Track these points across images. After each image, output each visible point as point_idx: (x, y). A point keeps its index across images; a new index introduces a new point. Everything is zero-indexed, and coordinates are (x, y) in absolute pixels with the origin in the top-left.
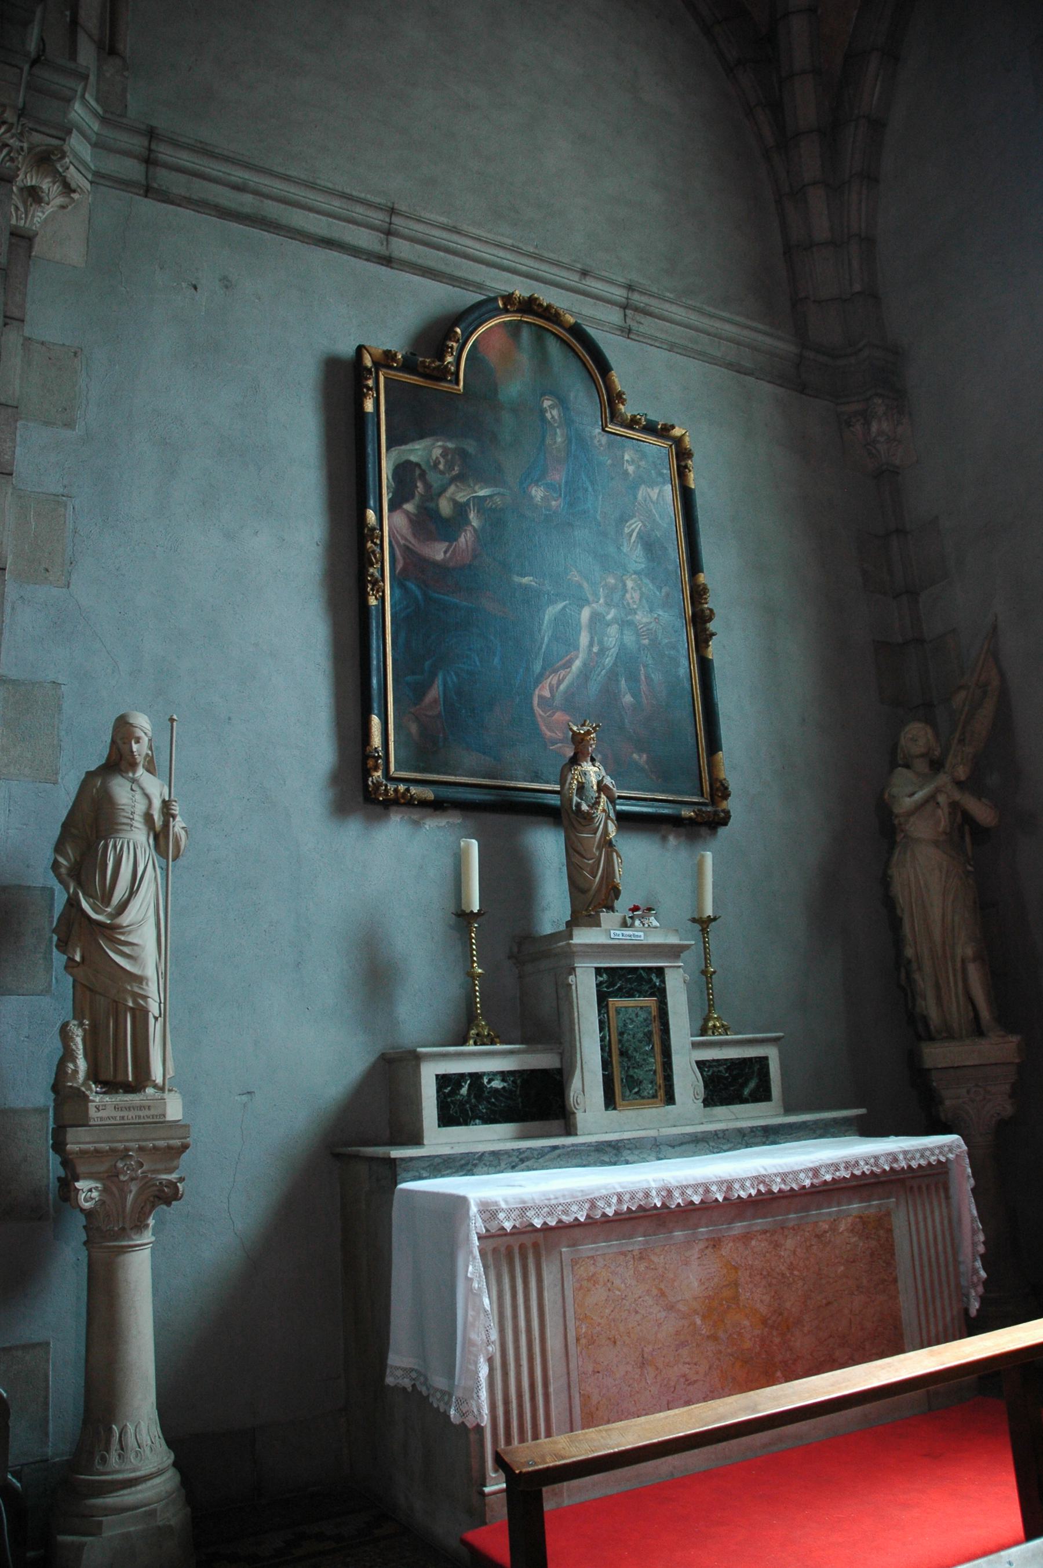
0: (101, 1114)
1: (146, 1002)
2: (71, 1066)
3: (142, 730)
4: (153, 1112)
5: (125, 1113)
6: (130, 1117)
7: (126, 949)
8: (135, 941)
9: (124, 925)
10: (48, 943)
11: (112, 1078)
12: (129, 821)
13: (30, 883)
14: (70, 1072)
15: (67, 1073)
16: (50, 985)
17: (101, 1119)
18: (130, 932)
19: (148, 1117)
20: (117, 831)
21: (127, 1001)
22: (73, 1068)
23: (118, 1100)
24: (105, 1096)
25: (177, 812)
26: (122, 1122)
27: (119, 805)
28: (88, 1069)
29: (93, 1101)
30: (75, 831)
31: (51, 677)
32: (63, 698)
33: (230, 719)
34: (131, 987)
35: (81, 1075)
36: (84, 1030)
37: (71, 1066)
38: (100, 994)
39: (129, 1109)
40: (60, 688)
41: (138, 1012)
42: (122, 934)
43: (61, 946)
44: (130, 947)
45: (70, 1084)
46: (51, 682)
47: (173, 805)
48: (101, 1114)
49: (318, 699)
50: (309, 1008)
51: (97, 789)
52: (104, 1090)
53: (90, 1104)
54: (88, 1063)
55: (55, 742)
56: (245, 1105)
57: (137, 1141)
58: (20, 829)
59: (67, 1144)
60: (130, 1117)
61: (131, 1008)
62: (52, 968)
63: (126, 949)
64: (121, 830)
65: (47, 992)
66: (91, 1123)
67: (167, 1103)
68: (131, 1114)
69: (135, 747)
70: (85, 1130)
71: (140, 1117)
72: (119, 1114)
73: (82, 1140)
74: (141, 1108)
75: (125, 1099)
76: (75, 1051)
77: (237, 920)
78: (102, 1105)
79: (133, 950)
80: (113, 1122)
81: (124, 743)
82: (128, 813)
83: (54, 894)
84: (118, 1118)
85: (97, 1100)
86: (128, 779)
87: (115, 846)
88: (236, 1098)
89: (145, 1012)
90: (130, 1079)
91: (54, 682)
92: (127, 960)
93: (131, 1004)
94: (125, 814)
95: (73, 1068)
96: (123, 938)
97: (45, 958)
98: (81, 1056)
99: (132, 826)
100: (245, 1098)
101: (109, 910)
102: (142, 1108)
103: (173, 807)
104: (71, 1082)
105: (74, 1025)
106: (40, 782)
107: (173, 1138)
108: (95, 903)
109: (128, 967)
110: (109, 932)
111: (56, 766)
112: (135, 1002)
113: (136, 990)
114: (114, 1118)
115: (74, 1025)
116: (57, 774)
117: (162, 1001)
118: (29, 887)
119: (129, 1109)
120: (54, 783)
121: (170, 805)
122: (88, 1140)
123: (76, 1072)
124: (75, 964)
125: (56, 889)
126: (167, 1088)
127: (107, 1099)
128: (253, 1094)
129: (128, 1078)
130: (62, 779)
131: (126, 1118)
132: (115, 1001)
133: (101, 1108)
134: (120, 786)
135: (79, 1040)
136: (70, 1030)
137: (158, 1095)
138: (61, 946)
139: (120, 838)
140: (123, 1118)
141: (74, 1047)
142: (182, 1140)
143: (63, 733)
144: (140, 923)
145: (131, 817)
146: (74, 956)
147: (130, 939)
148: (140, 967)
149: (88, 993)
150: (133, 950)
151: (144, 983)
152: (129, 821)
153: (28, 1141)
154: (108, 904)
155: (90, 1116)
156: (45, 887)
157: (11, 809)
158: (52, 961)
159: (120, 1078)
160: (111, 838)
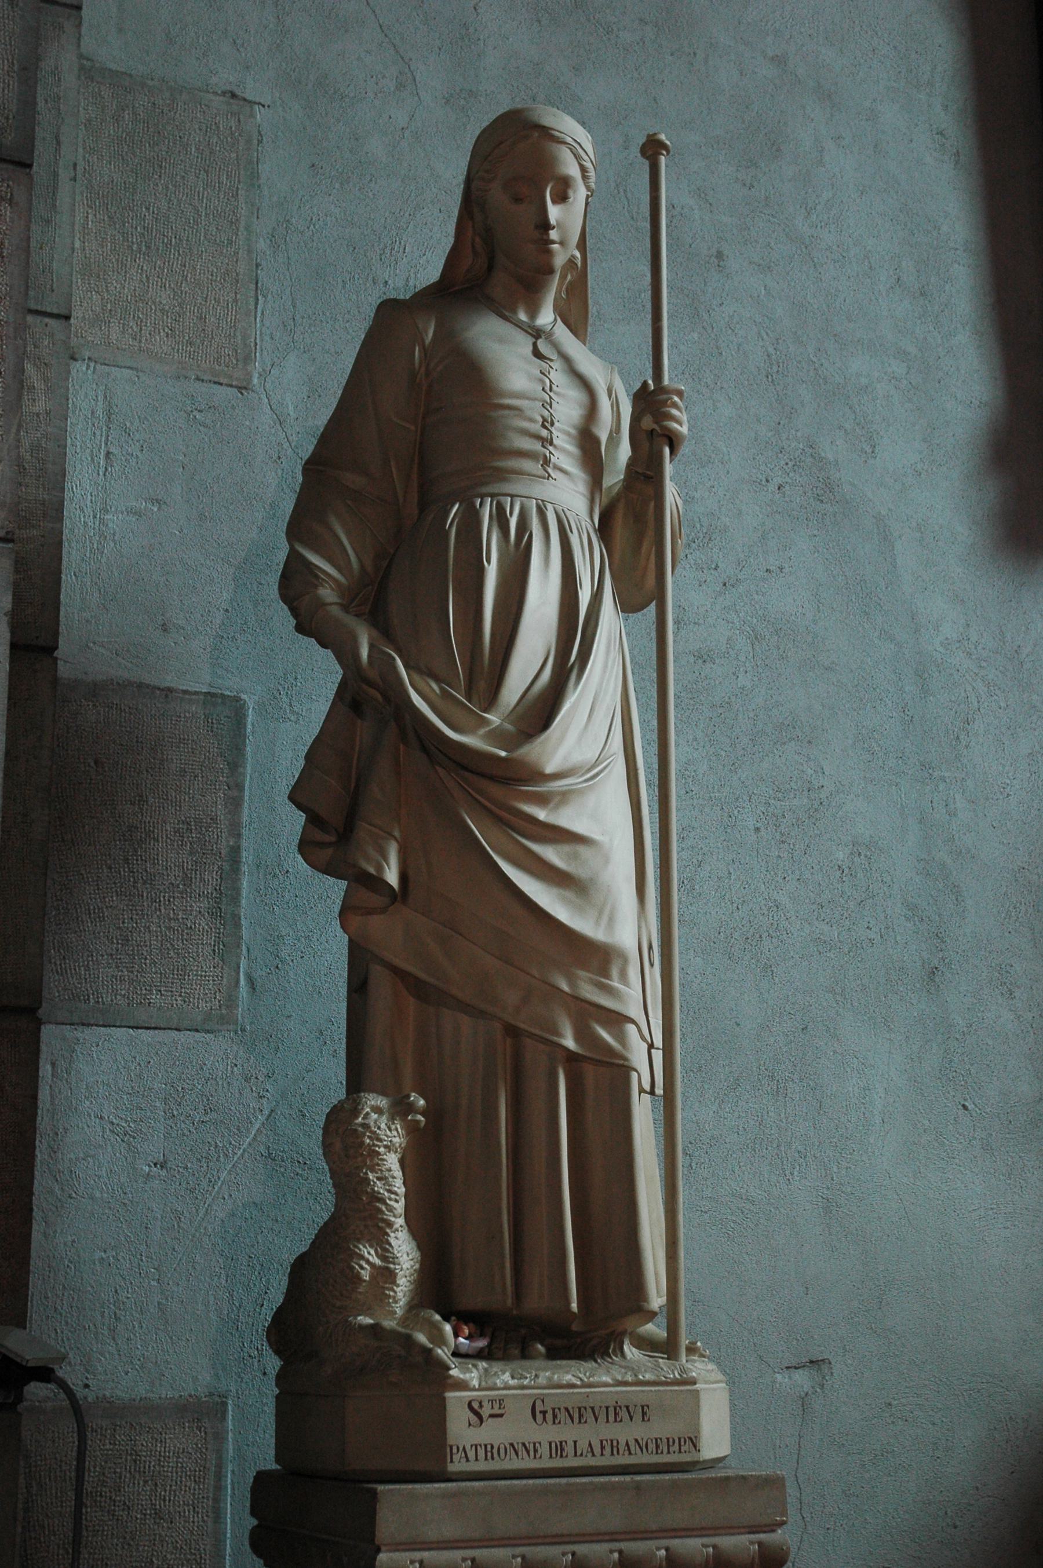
0: (491, 1433)
1: (621, 1038)
2: (370, 1253)
3: (577, 157)
4: (658, 1428)
5: (567, 1432)
6: (583, 1445)
7: (550, 853)
8: (578, 827)
9: (549, 770)
10: (226, 867)
11: (509, 1302)
12: (537, 446)
13: (169, 681)
14: (366, 1275)
15: (358, 1278)
16: (231, 1001)
17: (490, 1451)
18: (565, 797)
19: (643, 1447)
20: (502, 475)
21: (559, 1035)
22: (377, 1262)
23: (542, 1381)
24: (496, 1367)
25: (684, 430)
26: (558, 1463)
27: (502, 394)
28: (422, 1263)
29: (462, 1385)
30: (353, 480)
31: (225, 77)
32: (260, 142)
33: (720, 255)
34: (572, 981)
35: (403, 1288)
36: (412, 1129)
37: (370, 1253)
38: (465, 1008)
39: (579, 1414)
40: (252, 115)
41: (590, 1072)
42: (542, 800)
43: (322, 845)
44: (566, 848)
45: (366, 1320)
46: (224, 93)
47: (675, 405)
48: (491, 1433)
49: (945, 229)
50: (970, 1106)
51: (424, 349)
52: (481, 1343)
53: (449, 1395)
54: (420, 1247)
55: (242, 268)
56: (804, 1401)
57: (612, 1537)
58: (138, 514)
59: (378, 1550)
60: (583, 1445)
61: (571, 1058)
62: (239, 946)
63: (550, 853)
64: (520, 473)
65: (223, 1020)
66: (456, 1466)
67: (703, 1396)
68: (585, 1434)
69: (554, 212)
70: (446, 1495)
71: (614, 1447)
72: (545, 1434)
73: (432, 1534)
74: (617, 1412)
75: (568, 1378)
76: (383, 1201)
77: (763, 833)
78: (492, 1401)
79: (575, 857)
80: (527, 1463)
81: (517, 200)
82: (532, 420)
83: (245, 716)
84: (544, 1450)
85: (475, 1383)
86: (519, 325)
87: (501, 519)
88: (779, 1377)
89: (621, 1070)
90: (574, 1306)
91: (234, 95)
92: (555, 891)
93: (569, 1042)
94: (525, 424)
95: (377, 1262)
96: (542, 814)
97: (216, 913)
98: (400, 1221)
99: (546, 462)
100: (802, 1379)
101: (494, 718)
102: (589, 1415)
103: (674, 412)
104: (368, 1311)
105: (378, 1110)
106: (198, 379)
107: (731, 1529)
108: (445, 694)
109: (561, 913)
110: (496, 790)
111: (245, 338)
112: (583, 1034)
113: (589, 993)
114: (531, 1449)
115: (378, 1110)
116: (248, 359)
117: (658, 1041)
118: (170, 690)
119: (579, 1414)
120: (240, 389)
121: (664, 403)
122: (449, 1530)
123: (386, 1275)
124: (376, 900)
125: (251, 705)
126: (684, 1341)
127: (507, 1376)
128: (825, 1368)
129: (568, 1302)
130: (264, 375)
131: (569, 1449)
132: (513, 1032)
133: (485, 1412)
134: (501, 340)
135: (392, 1161)
136: (366, 1126)
137: (667, 1369)
138: (322, 845)
139: (512, 496)
140: (559, 1449)
141: (379, 1187)
142: (762, 1536)
143: (262, 244)
144: (593, 770)
145: (544, 433)
146: (380, 868)
147: (567, 818)
148: (601, 913)
149: (411, 1004)
150: (575, 857)
151: (615, 972)
152: (537, 446)
153: (158, 1515)
154: (491, 697)
155: (450, 1441)
156: (213, 695)
157: (113, 450)
158: (238, 925)
159: (536, 1302)
160: (483, 497)
